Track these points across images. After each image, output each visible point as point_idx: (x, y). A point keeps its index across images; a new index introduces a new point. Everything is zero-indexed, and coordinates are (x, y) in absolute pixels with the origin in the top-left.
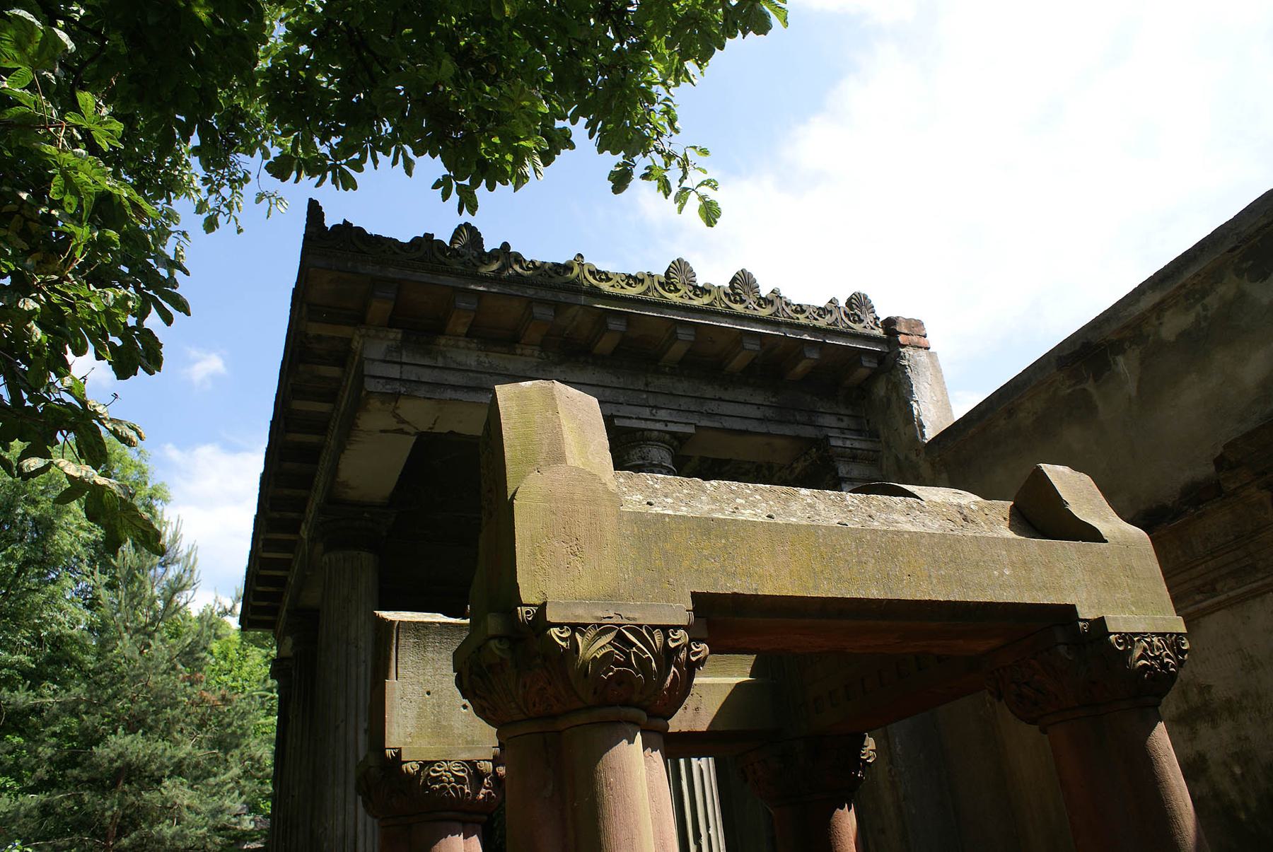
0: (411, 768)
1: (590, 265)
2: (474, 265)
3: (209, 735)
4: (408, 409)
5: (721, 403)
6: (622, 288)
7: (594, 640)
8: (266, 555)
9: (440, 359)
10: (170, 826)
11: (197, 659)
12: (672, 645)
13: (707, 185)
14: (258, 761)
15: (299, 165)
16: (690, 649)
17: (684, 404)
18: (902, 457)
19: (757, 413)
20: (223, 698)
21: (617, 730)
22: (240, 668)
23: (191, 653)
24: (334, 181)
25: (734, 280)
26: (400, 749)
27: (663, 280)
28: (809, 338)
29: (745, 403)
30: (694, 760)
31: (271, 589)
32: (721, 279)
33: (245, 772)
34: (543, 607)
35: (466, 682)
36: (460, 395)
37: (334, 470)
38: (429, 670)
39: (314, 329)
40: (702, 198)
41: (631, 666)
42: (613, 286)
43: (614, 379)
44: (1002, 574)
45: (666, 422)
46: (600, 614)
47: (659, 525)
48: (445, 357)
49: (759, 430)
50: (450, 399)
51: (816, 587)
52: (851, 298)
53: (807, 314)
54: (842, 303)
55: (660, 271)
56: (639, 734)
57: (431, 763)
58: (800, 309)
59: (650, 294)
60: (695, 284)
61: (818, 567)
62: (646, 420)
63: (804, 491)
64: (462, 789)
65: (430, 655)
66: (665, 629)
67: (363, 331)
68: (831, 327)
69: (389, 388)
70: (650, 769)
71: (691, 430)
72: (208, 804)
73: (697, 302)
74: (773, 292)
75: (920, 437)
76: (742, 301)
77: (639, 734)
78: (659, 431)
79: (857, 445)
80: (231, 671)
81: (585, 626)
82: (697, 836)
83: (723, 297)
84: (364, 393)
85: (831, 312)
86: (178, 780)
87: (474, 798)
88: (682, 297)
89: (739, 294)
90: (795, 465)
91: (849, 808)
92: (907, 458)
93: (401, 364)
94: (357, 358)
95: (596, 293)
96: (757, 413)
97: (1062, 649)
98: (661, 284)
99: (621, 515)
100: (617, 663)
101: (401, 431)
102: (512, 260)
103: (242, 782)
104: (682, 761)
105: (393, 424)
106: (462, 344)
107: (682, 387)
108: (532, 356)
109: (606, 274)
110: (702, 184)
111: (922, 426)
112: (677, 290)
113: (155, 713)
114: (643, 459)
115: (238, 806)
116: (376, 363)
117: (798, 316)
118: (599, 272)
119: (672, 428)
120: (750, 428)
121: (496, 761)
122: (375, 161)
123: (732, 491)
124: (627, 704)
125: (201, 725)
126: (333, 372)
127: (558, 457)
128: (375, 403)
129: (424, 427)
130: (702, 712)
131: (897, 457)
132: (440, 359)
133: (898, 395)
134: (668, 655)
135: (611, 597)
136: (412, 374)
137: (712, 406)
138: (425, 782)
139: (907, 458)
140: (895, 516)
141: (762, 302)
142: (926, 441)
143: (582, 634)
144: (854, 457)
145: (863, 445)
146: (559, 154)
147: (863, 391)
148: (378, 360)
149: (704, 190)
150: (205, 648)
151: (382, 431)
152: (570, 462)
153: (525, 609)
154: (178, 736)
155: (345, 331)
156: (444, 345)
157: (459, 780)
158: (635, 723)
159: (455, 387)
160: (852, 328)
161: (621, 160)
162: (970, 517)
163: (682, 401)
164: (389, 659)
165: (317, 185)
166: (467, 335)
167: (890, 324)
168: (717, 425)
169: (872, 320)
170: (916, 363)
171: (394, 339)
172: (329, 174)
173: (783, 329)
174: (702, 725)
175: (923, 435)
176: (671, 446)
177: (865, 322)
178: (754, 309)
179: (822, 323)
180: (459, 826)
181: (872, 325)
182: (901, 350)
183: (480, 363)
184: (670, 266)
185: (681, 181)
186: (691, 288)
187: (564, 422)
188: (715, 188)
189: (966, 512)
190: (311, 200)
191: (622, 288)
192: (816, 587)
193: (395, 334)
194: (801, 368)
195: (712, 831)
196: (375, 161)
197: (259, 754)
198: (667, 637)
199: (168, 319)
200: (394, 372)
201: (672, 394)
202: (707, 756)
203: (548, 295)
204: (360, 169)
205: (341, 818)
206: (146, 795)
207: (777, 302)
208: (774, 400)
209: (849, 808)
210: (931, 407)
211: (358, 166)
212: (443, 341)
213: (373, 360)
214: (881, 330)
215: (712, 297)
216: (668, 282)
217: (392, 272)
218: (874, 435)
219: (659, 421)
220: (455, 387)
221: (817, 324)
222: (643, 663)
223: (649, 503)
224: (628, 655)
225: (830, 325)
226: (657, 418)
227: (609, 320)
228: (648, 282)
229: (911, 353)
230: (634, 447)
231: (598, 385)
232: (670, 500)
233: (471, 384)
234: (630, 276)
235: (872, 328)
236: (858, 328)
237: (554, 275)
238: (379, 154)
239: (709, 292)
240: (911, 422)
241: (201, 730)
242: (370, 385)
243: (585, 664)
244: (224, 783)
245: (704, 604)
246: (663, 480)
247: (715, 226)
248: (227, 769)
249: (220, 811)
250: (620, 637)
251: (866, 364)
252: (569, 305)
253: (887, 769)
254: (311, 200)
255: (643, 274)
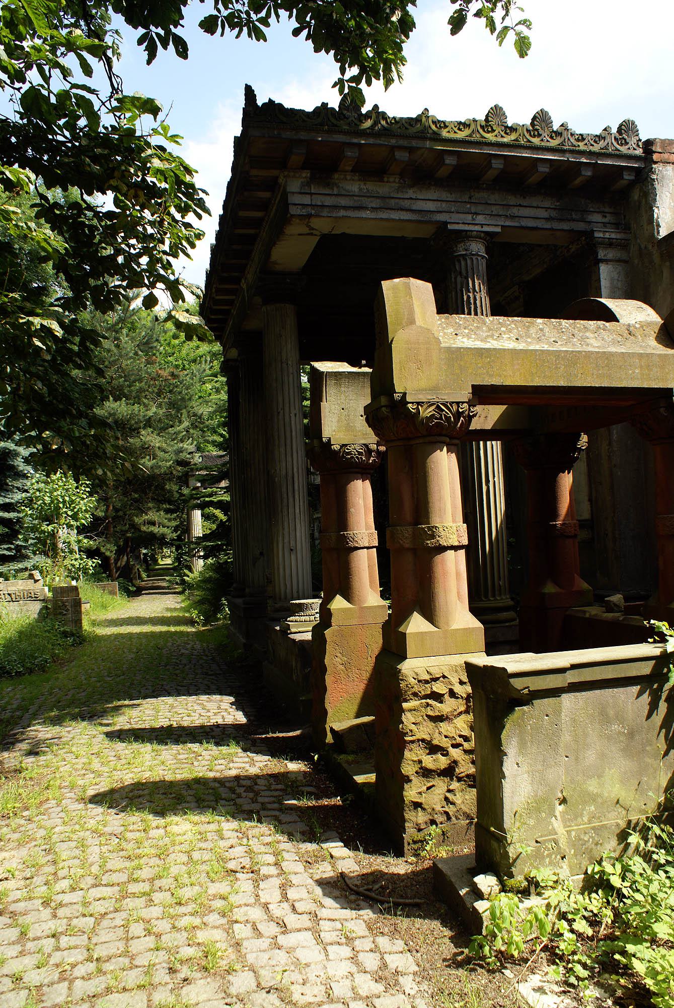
0: (336, 447)
1: (433, 116)
2: (355, 124)
3: (166, 400)
4: (316, 223)
5: (520, 208)
6: (455, 132)
7: (427, 409)
8: (218, 297)
9: (335, 189)
10: (149, 460)
11: (152, 348)
12: (461, 410)
13: (523, 24)
14: (200, 418)
15: (222, 22)
16: (470, 409)
17: (495, 210)
18: (643, 246)
19: (543, 214)
20: (173, 375)
21: (436, 445)
22: (180, 352)
23: (147, 343)
24: (250, 35)
25: (534, 119)
26: (330, 438)
27: (484, 123)
28: (585, 161)
29: (537, 207)
30: (489, 443)
31: (221, 317)
32: (525, 119)
33: (192, 424)
34: (405, 394)
35: (370, 421)
36: (350, 213)
37: (268, 254)
38: (343, 397)
39: (256, 173)
40: (518, 34)
41: (442, 420)
42: (449, 132)
43: (449, 195)
44: (634, 372)
45: (482, 225)
46: (430, 398)
47: (458, 353)
48: (338, 187)
49: (545, 227)
50: (343, 216)
51: (532, 381)
52: (621, 125)
53: (586, 141)
54: (614, 130)
55: (481, 117)
56: (445, 447)
57: (346, 445)
58: (582, 138)
59: (474, 136)
60: (506, 125)
61: (534, 371)
62: (469, 224)
63: (539, 321)
64: (362, 458)
65: (343, 389)
66: (458, 403)
67: (286, 173)
68: (603, 151)
69: (304, 212)
70: (449, 461)
71: (498, 230)
72: (172, 446)
73: (506, 139)
74: (562, 125)
75: (656, 234)
76: (539, 135)
77: (445, 447)
78: (477, 231)
79: (613, 236)
80: (173, 354)
81: (423, 403)
82: (488, 481)
83: (526, 133)
84: (289, 215)
85: (604, 138)
86: (150, 430)
87: (367, 462)
88: (496, 136)
89: (537, 130)
90: (570, 247)
91: (568, 473)
92: (646, 248)
93: (311, 194)
94: (282, 188)
95: (436, 137)
96: (543, 214)
97: (662, 410)
98: (482, 127)
99: (440, 349)
100: (436, 419)
101: (312, 234)
102: (380, 117)
103: (191, 431)
104: (481, 443)
105: (307, 231)
106: (348, 177)
107: (494, 198)
108: (394, 182)
109: (444, 122)
110: (520, 23)
111: (658, 226)
112: (493, 131)
113: (130, 386)
114: (466, 250)
115: (192, 448)
116: (295, 195)
117: (579, 143)
118: (439, 121)
119: (486, 229)
120: (540, 225)
121: (378, 444)
122: (278, 16)
123: (500, 323)
124: (441, 435)
125: (159, 394)
126: (266, 195)
127: (412, 322)
128: (296, 221)
129: (326, 231)
130: (489, 418)
131: (640, 246)
132: (335, 189)
133: (646, 201)
134: (458, 415)
135: (435, 389)
136: (318, 200)
137: (515, 211)
138: (343, 455)
139: (646, 248)
140: (587, 334)
141: (553, 135)
142: (660, 238)
143: (422, 406)
144: (610, 244)
145: (619, 236)
146: (412, 31)
147: (625, 193)
148: (296, 193)
149: (520, 28)
150: (157, 340)
151: (299, 235)
152: (418, 323)
153: (397, 395)
154: (146, 401)
155: (275, 173)
156: (337, 179)
157: (360, 453)
158: (444, 443)
159: (345, 208)
160: (619, 151)
161: (458, 8)
162: (633, 332)
163: (494, 208)
164: (322, 392)
165: (237, 37)
166: (352, 171)
167: (649, 144)
168: (516, 224)
169: (635, 142)
170: (663, 176)
171: (306, 177)
172: (245, 29)
173: (567, 155)
174: (489, 426)
175: (658, 232)
176: (485, 240)
177: (630, 144)
178: (548, 141)
179: (596, 148)
180: (360, 476)
181: (634, 146)
182: (653, 166)
183: (360, 189)
184: (489, 112)
185: (503, 19)
186: (503, 128)
187: (414, 302)
188: (529, 27)
189: (631, 329)
190: (246, 85)
191: (455, 132)
192: (532, 381)
193: (306, 174)
194: (578, 181)
195: (496, 479)
196: (278, 16)
197: (200, 412)
198: (459, 407)
199: (199, 217)
200: (306, 200)
201: (487, 203)
202: (496, 440)
203: (402, 142)
204: (267, 25)
205: (284, 464)
206: (131, 440)
207: (565, 133)
208: (558, 204)
209: (568, 473)
210: (668, 211)
211: (265, 21)
212: (336, 176)
213: (293, 193)
214: (641, 150)
215: (518, 134)
216: (487, 125)
217: (303, 135)
218: (627, 228)
219: (477, 224)
220: (345, 208)
221: (592, 149)
222: (448, 419)
223: (456, 334)
224: (441, 415)
225: (602, 149)
226: (476, 222)
227: (446, 157)
228: (473, 127)
229: (661, 169)
230: (460, 242)
231: (438, 200)
232: (467, 331)
233: (356, 204)
234: (460, 123)
235: (634, 149)
236: (623, 149)
237: (409, 127)
238: (281, 12)
239: (516, 130)
240: (651, 222)
241: (160, 396)
242: (293, 210)
243: (423, 419)
244: (180, 432)
245: (477, 389)
246: (464, 318)
247: (526, 57)
248: (180, 422)
249: (180, 451)
250: (438, 407)
251: (626, 177)
252: (418, 148)
253: (607, 448)
254: (246, 85)
255: (470, 120)
